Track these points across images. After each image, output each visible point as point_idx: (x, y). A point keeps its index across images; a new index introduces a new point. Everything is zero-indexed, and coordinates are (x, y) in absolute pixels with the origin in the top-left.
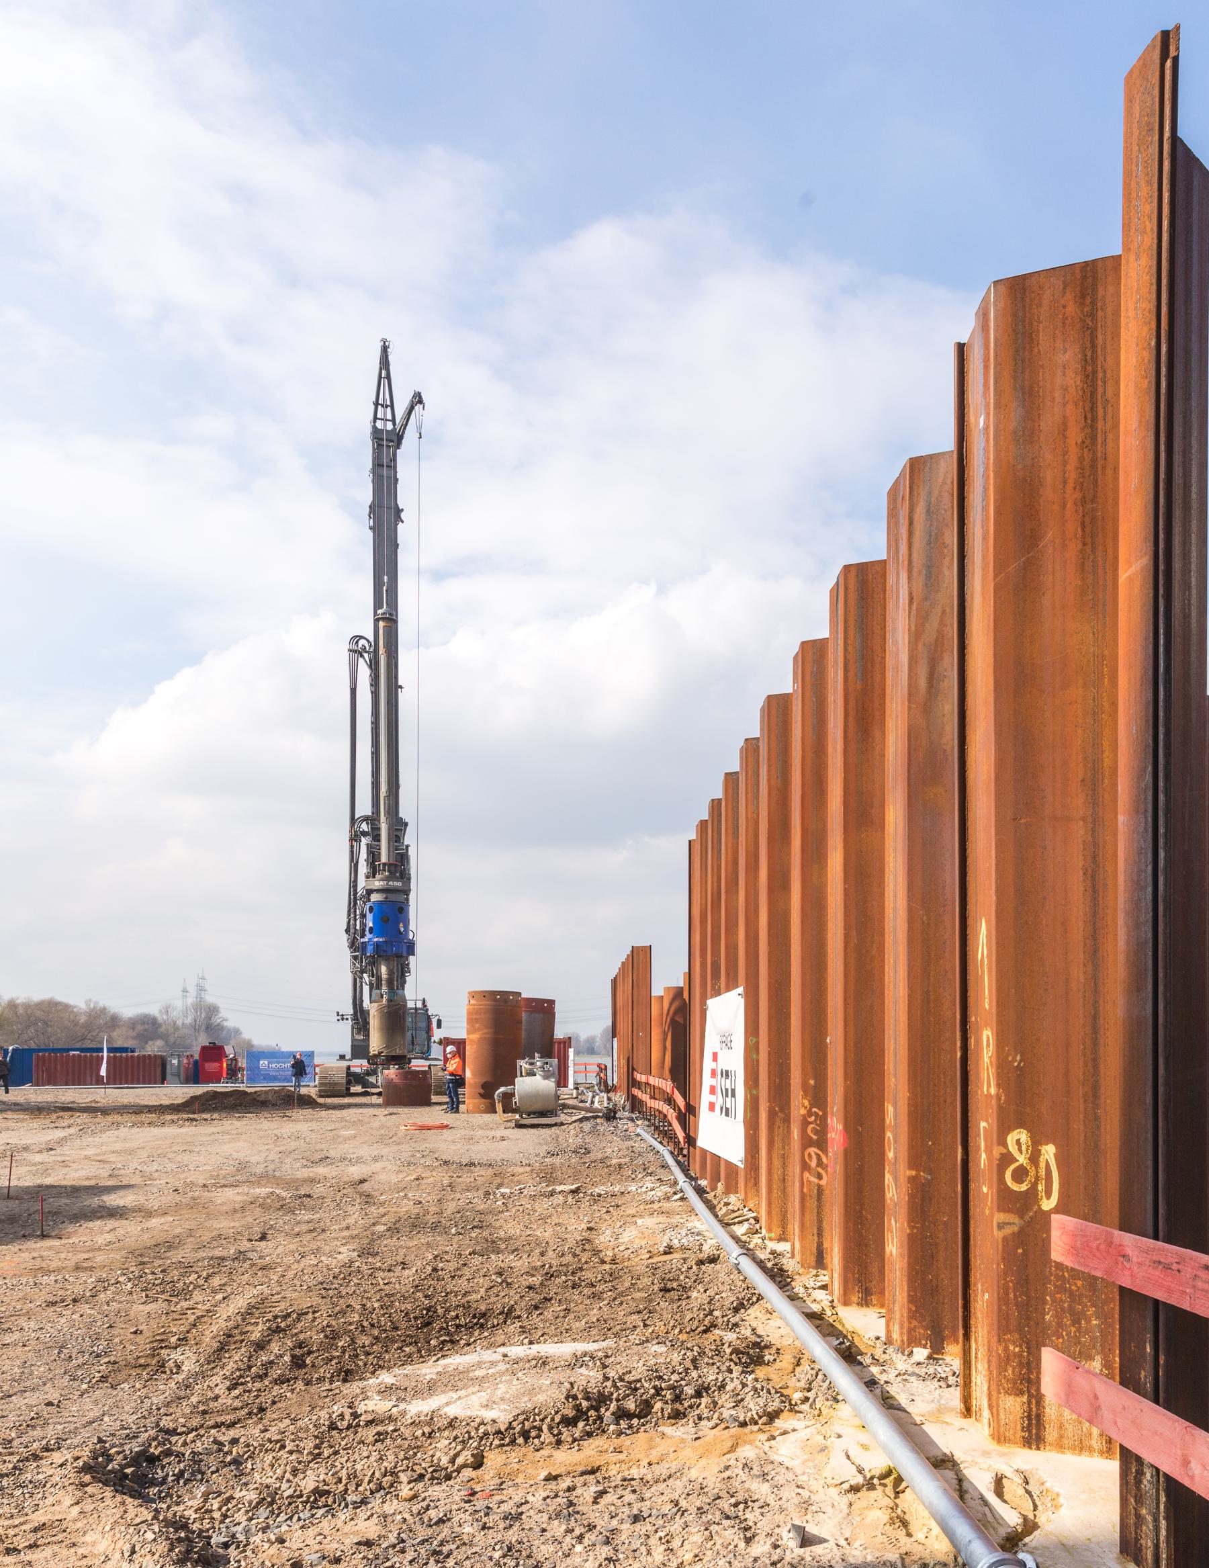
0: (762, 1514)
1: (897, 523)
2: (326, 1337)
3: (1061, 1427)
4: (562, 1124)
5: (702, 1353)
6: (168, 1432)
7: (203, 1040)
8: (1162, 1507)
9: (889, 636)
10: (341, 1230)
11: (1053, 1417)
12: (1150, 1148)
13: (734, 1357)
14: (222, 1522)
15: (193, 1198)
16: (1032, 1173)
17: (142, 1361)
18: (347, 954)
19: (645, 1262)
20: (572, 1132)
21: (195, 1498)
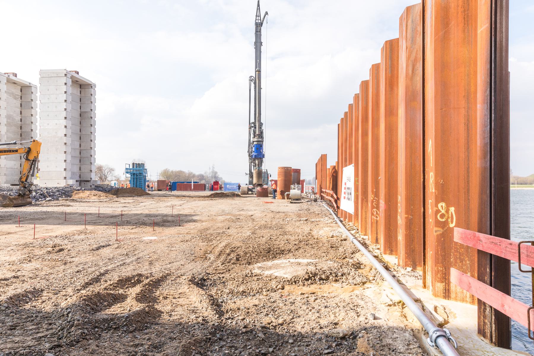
0: (362, 309)
1: (402, 27)
2: (244, 253)
3: (456, 293)
4: (302, 203)
5: (343, 264)
6: (208, 274)
7: (214, 180)
8: (493, 320)
9: (400, 59)
10: (247, 227)
11: (453, 290)
12: (489, 207)
13: (352, 266)
14: (221, 297)
15: (212, 218)
16: (447, 216)
17: (202, 256)
18: (248, 158)
19: (326, 240)
20: (305, 205)
21: (214, 290)
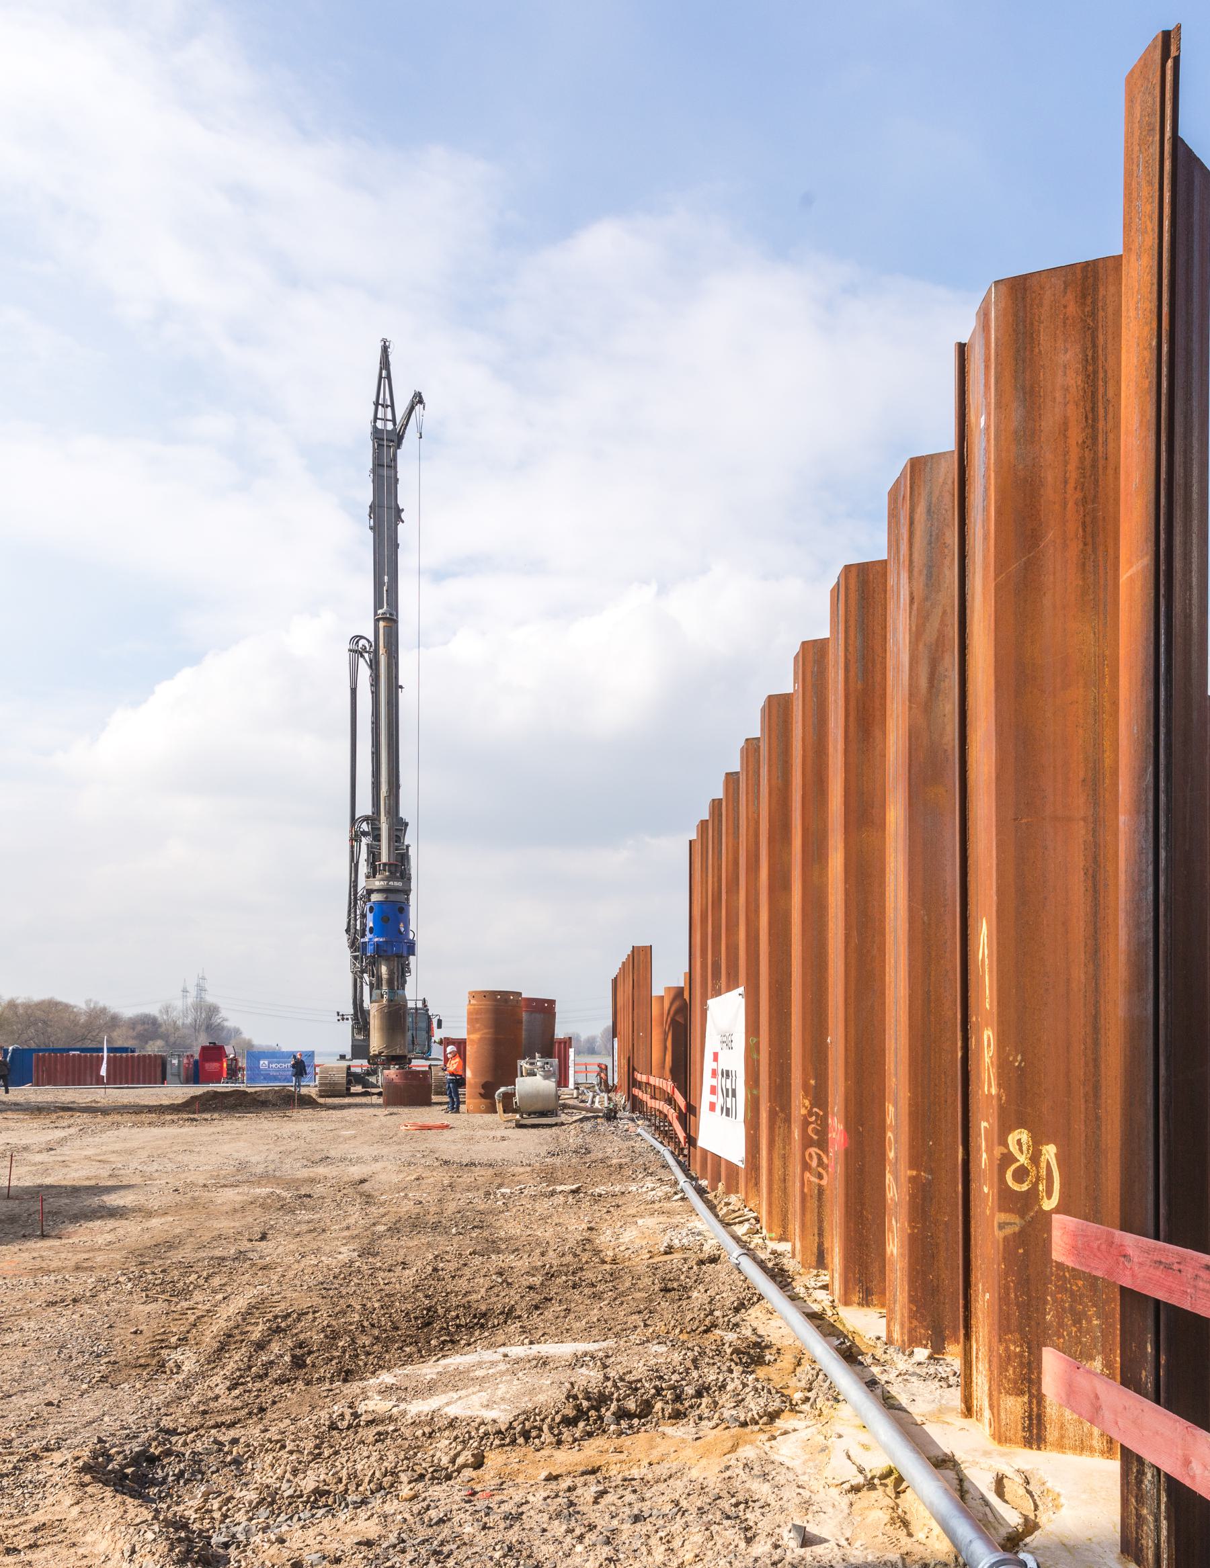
0: (763, 1514)
1: (898, 523)
2: (326, 1337)
3: (1062, 1427)
4: (563, 1124)
5: (702, 1353)
6: (168, 1432)
7: (204, 1040)
8: (1163, 1507)
9: (890, 636)
10: (342, 1230)
11: (1054, 1417)
12: (1151, 1148)
13: (734, 1357)
14: (222, 1522)
15: (193, 1198)
16: (1033, 1173)
17: (142, 1361)
18: (347, 954)
19: (646, 1262)
20: (573, 1132)
21: (195, 1498)
